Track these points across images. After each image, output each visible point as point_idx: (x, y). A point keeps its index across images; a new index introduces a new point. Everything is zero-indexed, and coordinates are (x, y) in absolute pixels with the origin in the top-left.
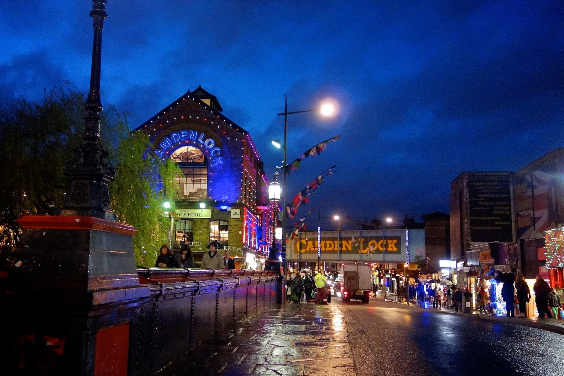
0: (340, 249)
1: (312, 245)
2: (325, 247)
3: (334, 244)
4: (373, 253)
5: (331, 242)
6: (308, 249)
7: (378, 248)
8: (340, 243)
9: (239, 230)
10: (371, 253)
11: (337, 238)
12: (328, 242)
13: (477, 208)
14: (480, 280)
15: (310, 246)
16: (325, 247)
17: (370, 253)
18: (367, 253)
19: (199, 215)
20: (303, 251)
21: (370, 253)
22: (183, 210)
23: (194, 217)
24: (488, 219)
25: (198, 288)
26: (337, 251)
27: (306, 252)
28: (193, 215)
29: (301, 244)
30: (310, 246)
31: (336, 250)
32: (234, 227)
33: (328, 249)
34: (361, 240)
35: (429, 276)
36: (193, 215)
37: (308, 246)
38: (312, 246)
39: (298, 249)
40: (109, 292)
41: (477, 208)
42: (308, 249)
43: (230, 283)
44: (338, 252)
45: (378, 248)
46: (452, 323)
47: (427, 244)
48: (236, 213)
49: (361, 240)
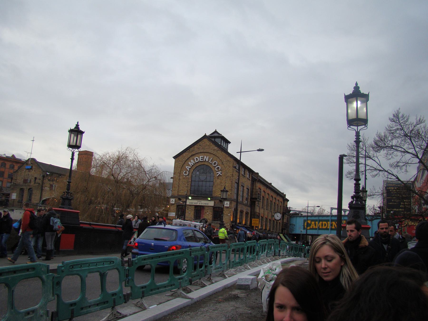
0: (331, 227)
1: (314, 224)
2: (322, 226)
3: (328, 224)
5: (326, 223)
6: (311, 227)
8: (331, 223)
9: (228, 213)
11: (329, 220)
12: (324, 223)
13: (391, 203)
15: (313, 225)
16: (322, 226)
19: (207, 204)
20: (308, 228)
22: (199, 201)
23: (205, 205)
24: (397, 210)
26: (317, 228)
27: (310, 229)
28: (204, 204)
29: (307, 223)
30: (313, 225)
31: (125, 265)
32: (226, 211)
33: (324, 227)
34: (343, 222)
35: (223, 241)
36: (204, 204)
37: (312, 225)
38: (314, 225)
39: (306, 227)
41: (391, 203)
42: (311, 227)
44: (330, 229)
46: (54, 228)
48: (227, 203)
49: (343, 222)
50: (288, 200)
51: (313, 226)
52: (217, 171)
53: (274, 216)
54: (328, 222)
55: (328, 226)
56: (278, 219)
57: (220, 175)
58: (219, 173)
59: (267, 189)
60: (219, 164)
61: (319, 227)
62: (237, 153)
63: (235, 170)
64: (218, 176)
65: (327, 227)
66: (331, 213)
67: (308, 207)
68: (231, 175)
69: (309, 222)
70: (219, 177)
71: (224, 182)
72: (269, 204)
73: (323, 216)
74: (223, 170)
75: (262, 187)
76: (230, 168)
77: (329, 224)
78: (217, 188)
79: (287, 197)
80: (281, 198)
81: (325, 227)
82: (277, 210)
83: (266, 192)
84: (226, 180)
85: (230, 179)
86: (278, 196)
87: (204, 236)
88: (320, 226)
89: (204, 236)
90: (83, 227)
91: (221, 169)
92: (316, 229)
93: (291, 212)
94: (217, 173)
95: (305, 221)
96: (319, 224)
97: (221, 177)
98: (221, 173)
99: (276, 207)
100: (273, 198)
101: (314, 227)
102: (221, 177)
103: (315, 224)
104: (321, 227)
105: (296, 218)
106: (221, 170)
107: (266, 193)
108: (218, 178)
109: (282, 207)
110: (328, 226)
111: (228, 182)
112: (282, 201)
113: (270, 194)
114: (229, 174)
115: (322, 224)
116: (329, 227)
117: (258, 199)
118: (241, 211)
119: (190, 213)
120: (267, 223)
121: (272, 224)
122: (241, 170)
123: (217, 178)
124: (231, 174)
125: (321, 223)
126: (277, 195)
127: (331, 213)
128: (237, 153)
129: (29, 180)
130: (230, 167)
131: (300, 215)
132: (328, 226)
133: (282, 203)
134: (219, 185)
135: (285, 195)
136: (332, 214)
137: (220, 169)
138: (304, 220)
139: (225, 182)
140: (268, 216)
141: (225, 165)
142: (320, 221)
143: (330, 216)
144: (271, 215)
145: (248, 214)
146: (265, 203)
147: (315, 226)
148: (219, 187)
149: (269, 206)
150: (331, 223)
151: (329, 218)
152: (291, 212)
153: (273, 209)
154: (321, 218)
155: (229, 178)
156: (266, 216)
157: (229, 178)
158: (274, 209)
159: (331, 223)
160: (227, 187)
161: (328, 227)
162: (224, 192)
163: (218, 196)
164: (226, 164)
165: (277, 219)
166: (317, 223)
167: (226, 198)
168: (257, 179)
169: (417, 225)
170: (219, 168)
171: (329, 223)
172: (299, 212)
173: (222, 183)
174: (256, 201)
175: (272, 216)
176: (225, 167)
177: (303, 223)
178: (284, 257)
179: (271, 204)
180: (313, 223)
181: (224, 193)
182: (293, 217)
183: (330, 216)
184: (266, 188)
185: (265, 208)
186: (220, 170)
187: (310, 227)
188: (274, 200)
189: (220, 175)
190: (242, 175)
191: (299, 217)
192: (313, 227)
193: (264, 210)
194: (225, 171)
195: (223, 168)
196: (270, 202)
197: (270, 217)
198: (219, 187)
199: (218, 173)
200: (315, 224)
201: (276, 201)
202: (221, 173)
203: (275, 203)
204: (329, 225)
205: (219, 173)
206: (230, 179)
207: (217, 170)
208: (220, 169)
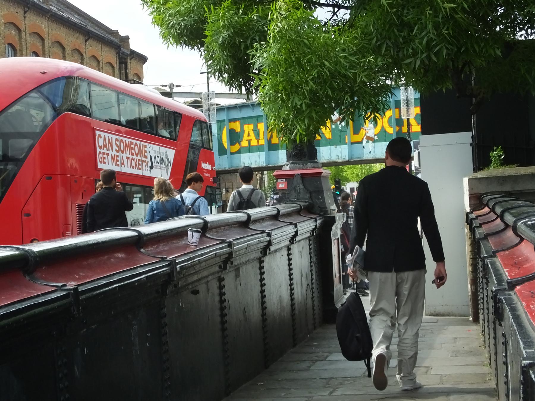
1: (252, 133)
4: (374, 141)
7: (383, 129)
10: (370, 142)
14: (178, 265)
15: (249, 135)
17: (368, 142)
18: (361, 142)
21: (368, 142)
25: (230, 255)
30: (249, 135)
31: (396, 109)
37: (246, 137)
38: (252, 136)
40: (303, 396)
42: (244, 144)
43: (245, 224)
45: (383, 129)
47: (320, 147)
51: (250, 138)
59: (27, 15)
61: (269, 141)
62: (201, 73)
69: (237, 126)
83: (22, 28)
86: (90, 42)
90: (404, 126)
92: (259, 148)
101: (254, 143)
103: (256, 131)
107: (23, 34)
113: (45, 36)
119: (148, 152)
126: (25, 12)
128: (201, 73)
129: (205, 142)
147: (258, 137)
169: (101, 195)
178: (465, 17)
180: (248, 128)
187: (240, 144)
192: (249, 141)
200: (256, 131)
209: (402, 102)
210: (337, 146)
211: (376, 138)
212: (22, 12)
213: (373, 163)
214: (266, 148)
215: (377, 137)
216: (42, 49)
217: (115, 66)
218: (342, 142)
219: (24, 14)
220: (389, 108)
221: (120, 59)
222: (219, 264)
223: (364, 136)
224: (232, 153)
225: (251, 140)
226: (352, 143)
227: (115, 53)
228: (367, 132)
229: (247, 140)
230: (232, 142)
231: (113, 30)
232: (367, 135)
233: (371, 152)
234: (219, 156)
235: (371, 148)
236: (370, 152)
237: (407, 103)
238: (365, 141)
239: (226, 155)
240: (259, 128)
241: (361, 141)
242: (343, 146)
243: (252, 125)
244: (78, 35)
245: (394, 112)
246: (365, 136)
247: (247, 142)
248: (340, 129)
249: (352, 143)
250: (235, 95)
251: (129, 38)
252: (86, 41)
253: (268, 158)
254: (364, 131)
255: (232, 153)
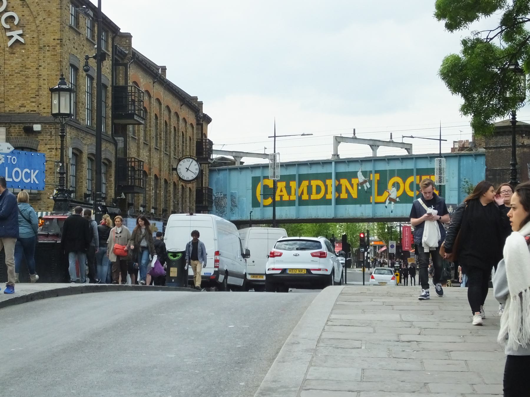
0: (337, 195)
1: (284, 190)
2: (310, 193)
3: (326, 186)
4: (395, 202)
5: (320, 183)
7: (404, 192)
8: (337, 183)
10: (393, 203)
12: (314, 183)
15: (281, 191)
16: (310, 193)
17: (390, 203)
18: (385, 203)
21: (390, 203)
30: (281, 191)
33: (314, 197)
37: (278, 192)
38: (285, 192)
44: (333, 202)
50: (208, 120)
51: (282, 194)
52: (6, 30)
53: (176, 169)
54: (328, 182)
55: (326, 192)
56: (191, 178)
57: (17, 41)
58: (15, 34)
60: (11, 5)
61: (300, 198)
63: (67, 25)
64: (11, 46)
65: (325, 196)
66: (336, 155)
67: (275, 137)
68: (54, 39)
70: (17, 49)
71: (32, 64)
72: (161, 134)
73: (361, 161)
74: (29, 27)
75: (142, 80)
76: (50, 19)
77: (329, 187)
78: (13, 87)
79: (205, 110)
80: (191, 112)
81: (319, 196)
82: (183, 151)
83: (152, 96)
84: (41, 57)
85: (52, 55)
87: (342, 279)
88: (302, 193)
89: (342, 279)
91: (22, 22)
92: (291, 203)
93: (214, 156)
94: (9, 34)
95: (256, 181)
96: (299, 187)
97: (21, 49)
98: (20, 35)
99: (181, 142)
100: (172, 114)
101: (286, 198)
102: (24, 49)
103: (288, 189)
104: (305, 197)
105: (230, 174)
106: (19, 26)
108: (14, 54)
109: (193, 140)
110: (329, 191)
111: (48, 64)
112: (194, 123)
113: (162, 102)
114: (49, 39)
115: (310, 187)
116: (331, 196)
117: (136, 117)
118: (90, 156)
120: (160, 191)
121: (172, 196)
122: (84, 25)
123: (11, 53)
124: (56, 38)
125: (305, 183)
127: (336, 155)
130: (49, 14)
131: (237, 165)
132: (326, 192)
133: (195, 129)
134: (16, 75)
135: (201, 104)
136: (338, 155)
137: (16, 22)
138: (252, 177)
139: (37, 66)
140: (160, 170)
141: (32, 7)
142: (302, 178)
143: (333, 163)
144: (167, 166)
145: (111, 166)
146: (150, 130)
147: (289, 193)
148: (20, 82)
149: (161, 137)
150: (337, 183)
151: (332, 169)
152: (214, 156)
153: (172, 147)
154: (304, 171)
155: (48, 51)
156: (155, 171)
157: (48, 51)
158: (175, 148)
159: (335, 184)
160: (44, 80)
161: (328, 197)
162: (62, 93)
163: (17, 111)
164: (36, 4)
165: (185, 179)
166: (293, 184)
167: (69, 112)
168: (126, 54)
170: (12, 18)
171: (331, 183)
172: (234, 154)
173: (26, 68)
174: (129, 124)
175: (169, 170)
176: (34, 13)
177: (251, 186)
179: (166, 134)
181: (61, 98)
182: (219, 170)
183: (333, 163)
184: (151, 81)
185: (153, 145)
186: (17, 25)
188: (182, 124)
189: (17, 41)
190: (87, 39)
191: (236, 169)
192: (281, 196)
193: (150, 150)
194: (34, 28)
195: (28, 18)
196: (163, 126)
197: (164, 175)
198: (17, 82)
199: (12, 36)
200: (288, 189)
201: (178, 123)
202: (20, 35)
203: (177, 129)
204: (332, 190)
205: (15, 34)
206: (52, 55)
207: (7, 26)
208: (16, 22)
209: (435, 170)
210: (362, 205)
211: (398, 200)
212: (152, 83)
213: (304, 223)
214: (297, 203)
215: (399, 199)
216: (160, 112)
217: (194, 127)
218: (367, 201)
219: (154, 83)
220: (412, 175)
221: (198, 121)
222: (400, 284)
223: (387, 198)
224: (264, 206)
225: (283, 195)
226: (376, 203)
227: (194, 116)
228: (390, 195)
229: (279, 196)
230: (265, 197)
231: (192, 96)
232: (390, 197)
233: (393, 211)
234: (252, 208)
235: (392, 208)
236: (392, 212)
237: (440, 172)
238: (388, 201)
239: (260, 207)
240: (291, 185)
241: (384, 201)
242: (367, 206)
243: (285, 183)
244: (177, 100)
245: (415, 179)
246: (388, 198)
247: (279, 197)
248: (366, 190)
249: (376, 203)
250: (262, 155)
251: (203, 104)
252: (181, 106)
253: (298, 211)
254: (388, 193)
255: (264, 206)
